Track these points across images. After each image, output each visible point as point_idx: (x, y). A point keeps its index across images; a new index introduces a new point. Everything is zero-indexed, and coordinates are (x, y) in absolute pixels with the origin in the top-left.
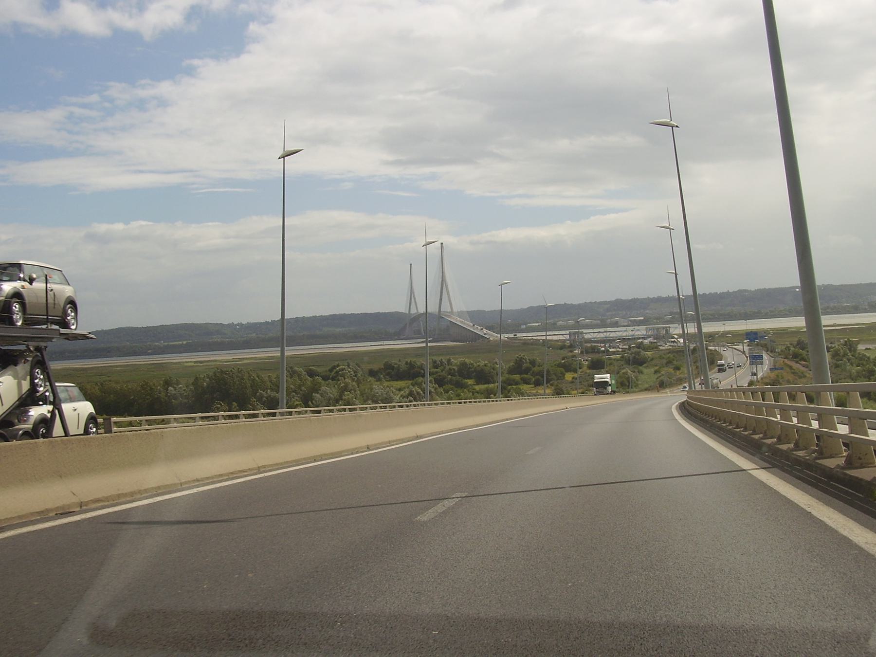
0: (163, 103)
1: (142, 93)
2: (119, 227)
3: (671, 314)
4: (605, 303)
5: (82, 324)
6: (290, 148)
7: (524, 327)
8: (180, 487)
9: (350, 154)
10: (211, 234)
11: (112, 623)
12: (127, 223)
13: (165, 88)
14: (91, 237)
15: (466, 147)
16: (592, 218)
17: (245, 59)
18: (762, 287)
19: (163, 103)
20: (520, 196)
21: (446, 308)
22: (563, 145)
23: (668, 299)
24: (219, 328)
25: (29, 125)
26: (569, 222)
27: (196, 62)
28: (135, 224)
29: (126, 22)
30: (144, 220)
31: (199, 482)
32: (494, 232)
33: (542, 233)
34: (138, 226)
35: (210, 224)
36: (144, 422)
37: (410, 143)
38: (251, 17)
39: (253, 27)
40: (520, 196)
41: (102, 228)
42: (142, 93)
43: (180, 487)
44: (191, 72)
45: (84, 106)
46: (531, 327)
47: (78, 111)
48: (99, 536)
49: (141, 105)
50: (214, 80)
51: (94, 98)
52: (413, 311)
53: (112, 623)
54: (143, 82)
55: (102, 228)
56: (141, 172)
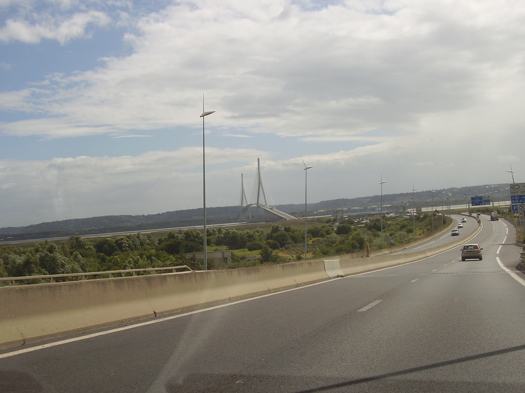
0: (88, 85)
1: (74, 79)
2: (69, 160)
3: (409, 202)
4: (368, 197)
6: (206, 111)
7: (315, 212)
10: (126, 163)
11: (180, 382)
12: (74, 158)
13: (89, 75)
14: (51, 166)
15: (273, 106)
16: (356, 149)
17: (134, 57)
18: (465, 186)
19: (88, 85)
20: (312, 136)
21: (262, 202)
22: (333, 104)
24: (130, 218)
25: (11, 99)
26: (342, 151)
27: (106, 59)
28: (79, 158)
29: (49, 34)
30: (86, 156)
31: (230, 300)
32: (297, 158)
33: (326, 158)
34: (81, 159)
35: (125, 157)
36: (174, 270)
37: (240, 105)
38: (124, 30)
39: (127, 36)
40: (312, 136)
41: (59, 161)
42: (74, 79)
44: (103, 65)
45: (40, 87)
46: (320, 212)
47: (37, 90)
48: (167, 333)
49: (69, 86)
50: (117, 71)
51: (46, 82)
52: (245, 205)
53: (180, 382)
54: (75, 72)
55: (59, 161)
56: (80, 126)
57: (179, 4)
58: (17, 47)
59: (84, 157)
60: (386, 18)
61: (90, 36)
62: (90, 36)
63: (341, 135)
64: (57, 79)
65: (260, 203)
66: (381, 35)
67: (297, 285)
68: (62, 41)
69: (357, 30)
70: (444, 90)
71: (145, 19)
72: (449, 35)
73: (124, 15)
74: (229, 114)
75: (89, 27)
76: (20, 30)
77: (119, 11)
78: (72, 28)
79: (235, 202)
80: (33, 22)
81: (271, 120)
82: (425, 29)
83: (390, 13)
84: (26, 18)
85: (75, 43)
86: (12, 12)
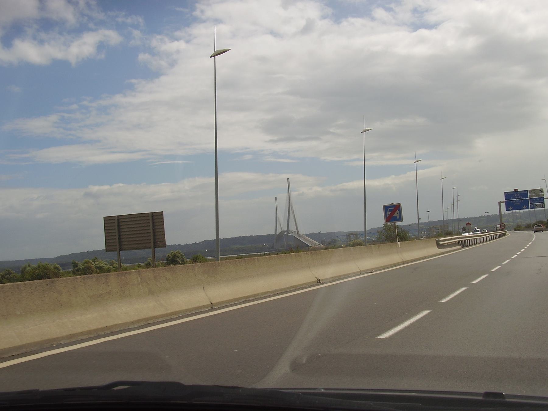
2: (106, 187)
5: (175, 236)
8: (347, 276)
9: (241, 135)
13: (119, 99)
14: (88, 195)
15: (313, 128)
16: (408, 173)
23: (494, 216)
25: (39, 125)
26: (394, 176)
27: (133, 81)
28: (116, 186)
32: (345, 184)
34: (119, 186)
37: (279, 127)
39: (143, 57)
41: (95, 189)
43: (347, 276)
44: (131, 87)
47: (66, 115)
50: (147, 94)
55: (95, 189)
57: (204, 21)
58: (27, 69)
59: (121, 185)
60: (424, 32)
61: (103, 56)
62: (103, 56)
63: (390, 159)
64: (85, 103)
65: (290, 229)
66: (422, 50)
67: (212, 307)
68: (73, 60)
69: (390, 44)
70: (505, 111)
71: (158, 37)
72: (497, 48)
73: (136, 33)
74: (269, 138)
75: (101, 46)
76: (29, 51)
77: (130, 28)
78: (83, 47)
79: (269, 230)
80: (41, 42)
81: (314, 143)
82: (471, 43)
83: (430, 27)
84: (34, 38)
85: (86, 64)
86: (15, 30)
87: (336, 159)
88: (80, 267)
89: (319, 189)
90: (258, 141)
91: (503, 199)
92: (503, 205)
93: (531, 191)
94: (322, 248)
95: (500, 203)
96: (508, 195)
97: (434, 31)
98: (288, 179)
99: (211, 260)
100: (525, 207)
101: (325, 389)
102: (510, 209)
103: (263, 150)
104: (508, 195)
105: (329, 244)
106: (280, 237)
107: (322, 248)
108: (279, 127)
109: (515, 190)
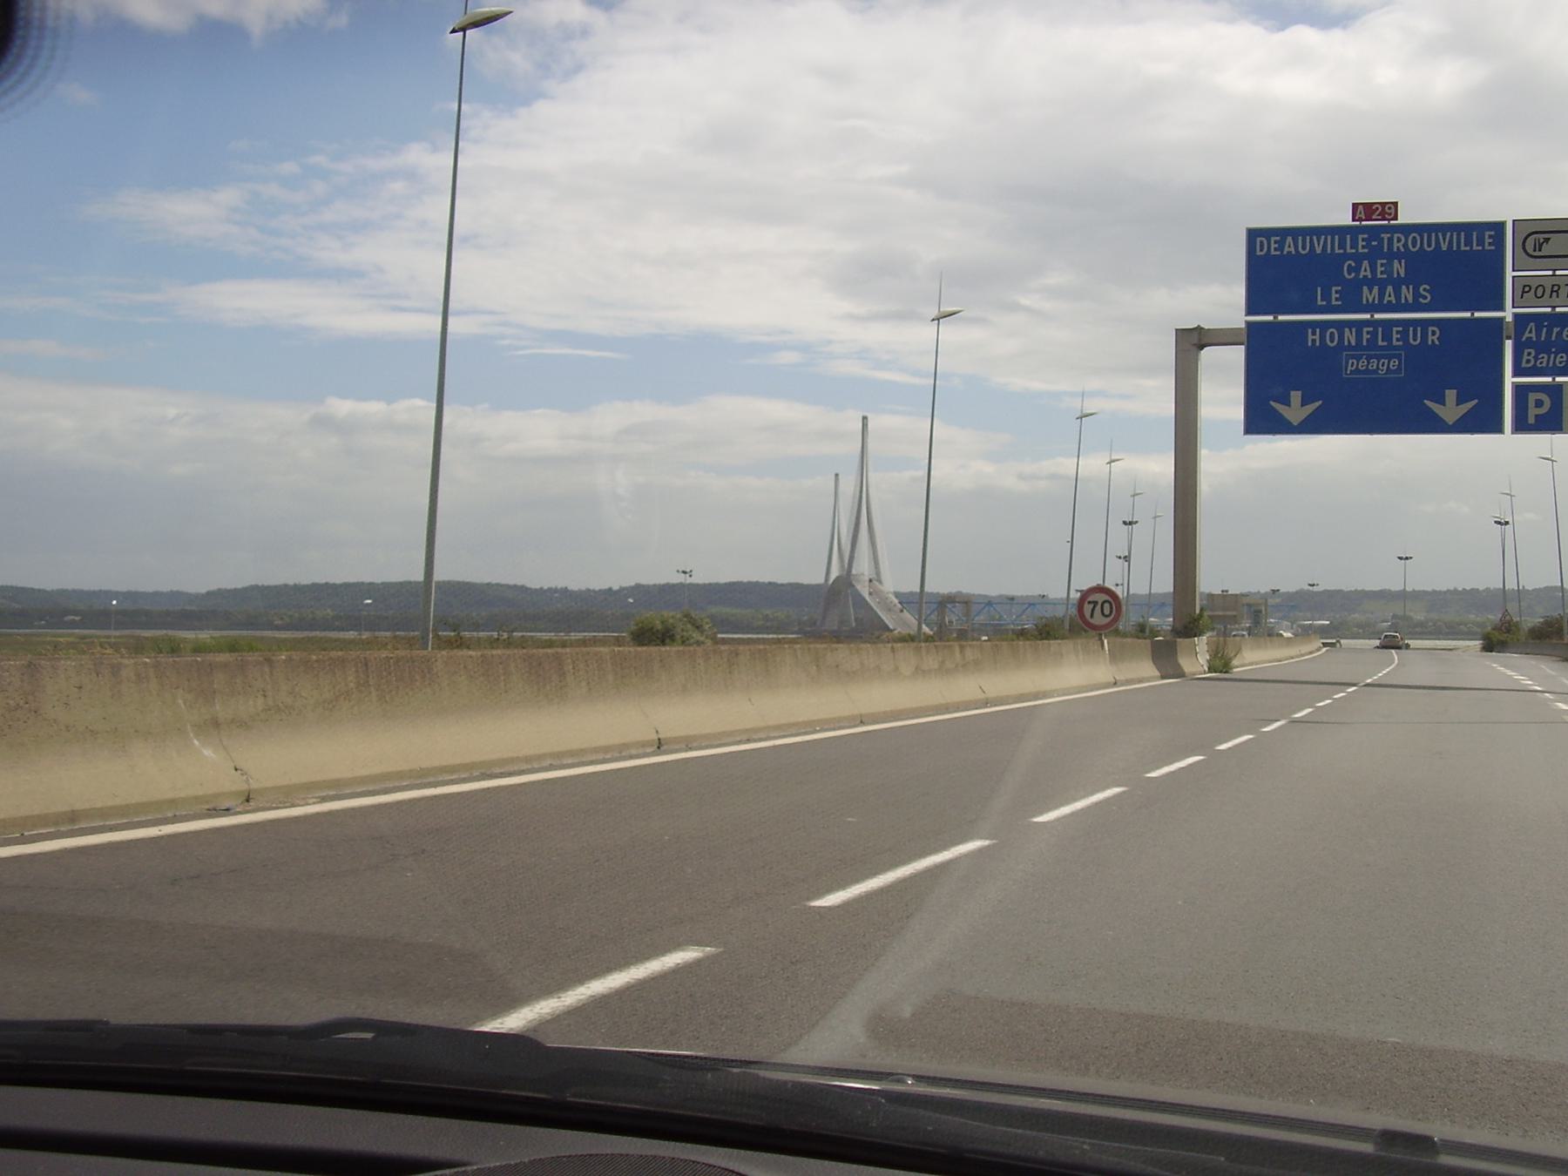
2: (375, 408)
14: (323, 423)
25: (191, 213)
28: (403, 405)
41: (342, 407)
55: (342, 407)
60: (1304, 35)
64: (320, 159)
82: (1448, 80)
87: (1037, 385)
88: (1423, 631)
89: (989, 468)
90: (813, 313)
91: (1224, 300)
92: (1224, 385)
93: (1541, 237)
94: (928, 639)
95: (1193, 341)
96: (1284, 266)
97: (1337, 34)
98: (865, 418)
99: (478, 644)
100: (1450, 410)
101: (919, 1078)
102: (1295, 411)
103: (830, 342)
104: (1284, 266)
105: (955, 626)
106: (840, 591)
107: (928, 639)
108: (869, 276)
109: (1364, 210)
